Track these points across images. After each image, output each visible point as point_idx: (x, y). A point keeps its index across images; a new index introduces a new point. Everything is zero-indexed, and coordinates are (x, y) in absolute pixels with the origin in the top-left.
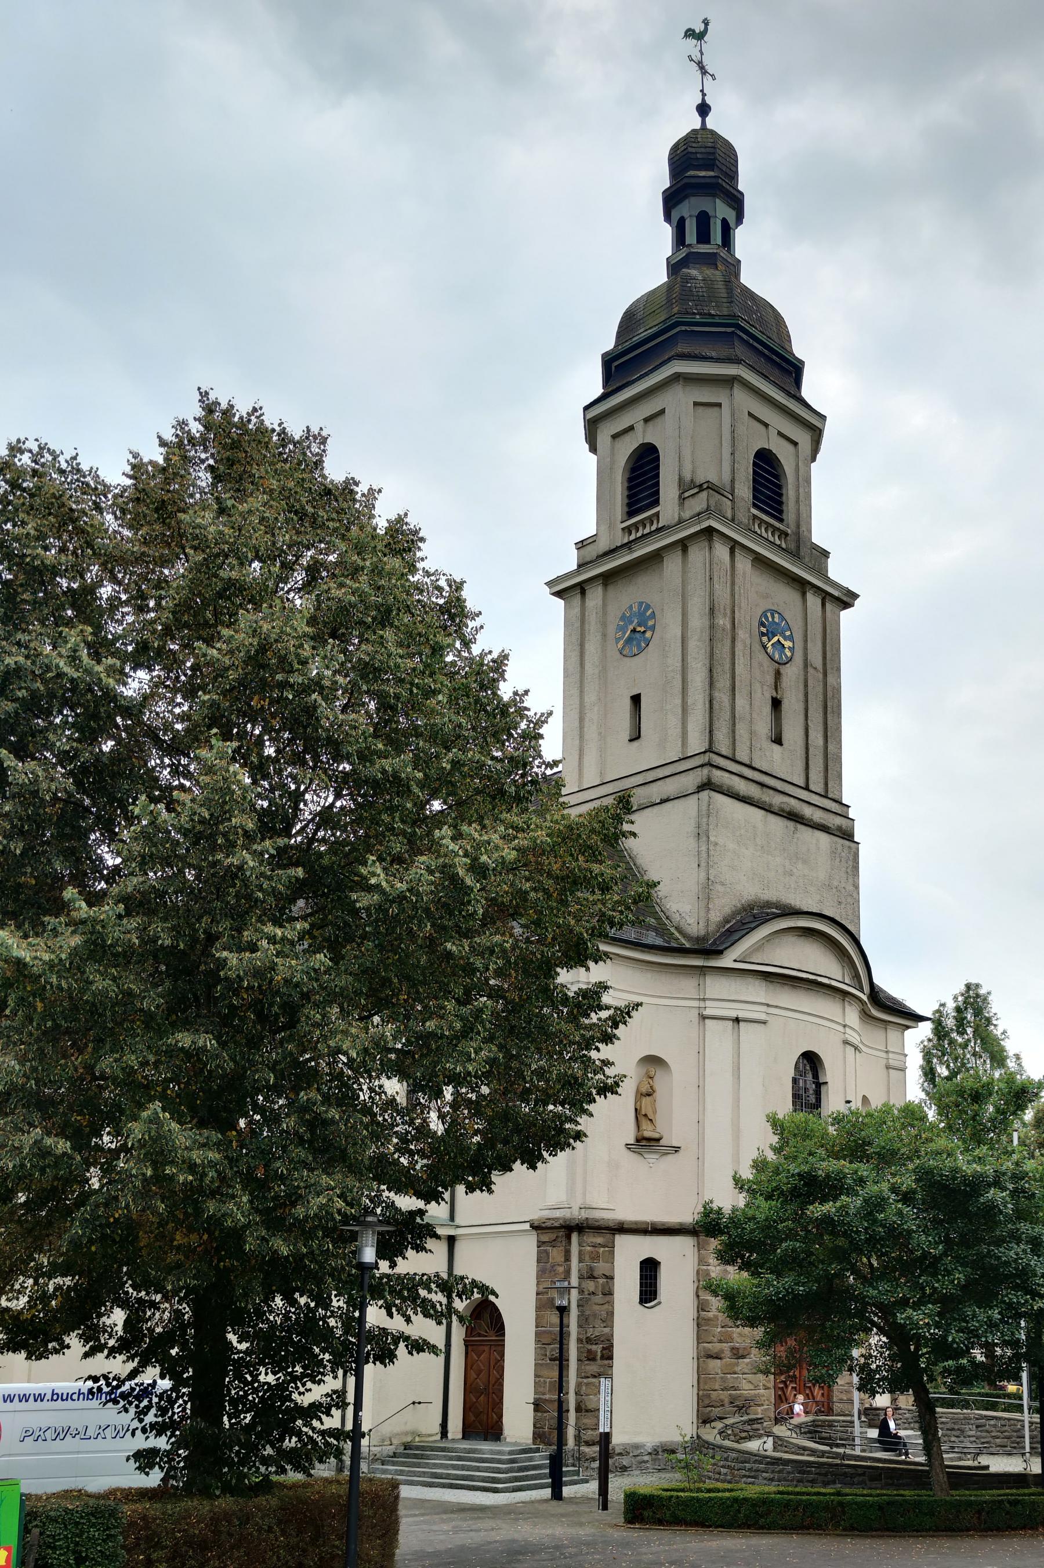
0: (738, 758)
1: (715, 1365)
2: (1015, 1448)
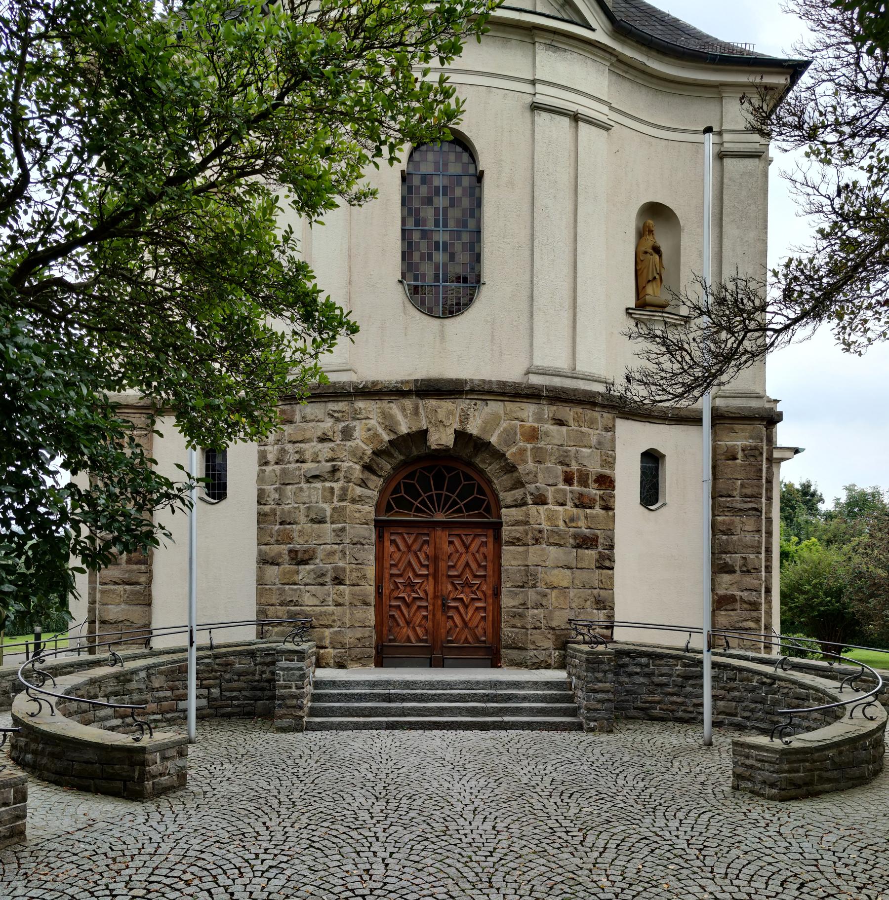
0: (566, 121)
1: (272, 571)
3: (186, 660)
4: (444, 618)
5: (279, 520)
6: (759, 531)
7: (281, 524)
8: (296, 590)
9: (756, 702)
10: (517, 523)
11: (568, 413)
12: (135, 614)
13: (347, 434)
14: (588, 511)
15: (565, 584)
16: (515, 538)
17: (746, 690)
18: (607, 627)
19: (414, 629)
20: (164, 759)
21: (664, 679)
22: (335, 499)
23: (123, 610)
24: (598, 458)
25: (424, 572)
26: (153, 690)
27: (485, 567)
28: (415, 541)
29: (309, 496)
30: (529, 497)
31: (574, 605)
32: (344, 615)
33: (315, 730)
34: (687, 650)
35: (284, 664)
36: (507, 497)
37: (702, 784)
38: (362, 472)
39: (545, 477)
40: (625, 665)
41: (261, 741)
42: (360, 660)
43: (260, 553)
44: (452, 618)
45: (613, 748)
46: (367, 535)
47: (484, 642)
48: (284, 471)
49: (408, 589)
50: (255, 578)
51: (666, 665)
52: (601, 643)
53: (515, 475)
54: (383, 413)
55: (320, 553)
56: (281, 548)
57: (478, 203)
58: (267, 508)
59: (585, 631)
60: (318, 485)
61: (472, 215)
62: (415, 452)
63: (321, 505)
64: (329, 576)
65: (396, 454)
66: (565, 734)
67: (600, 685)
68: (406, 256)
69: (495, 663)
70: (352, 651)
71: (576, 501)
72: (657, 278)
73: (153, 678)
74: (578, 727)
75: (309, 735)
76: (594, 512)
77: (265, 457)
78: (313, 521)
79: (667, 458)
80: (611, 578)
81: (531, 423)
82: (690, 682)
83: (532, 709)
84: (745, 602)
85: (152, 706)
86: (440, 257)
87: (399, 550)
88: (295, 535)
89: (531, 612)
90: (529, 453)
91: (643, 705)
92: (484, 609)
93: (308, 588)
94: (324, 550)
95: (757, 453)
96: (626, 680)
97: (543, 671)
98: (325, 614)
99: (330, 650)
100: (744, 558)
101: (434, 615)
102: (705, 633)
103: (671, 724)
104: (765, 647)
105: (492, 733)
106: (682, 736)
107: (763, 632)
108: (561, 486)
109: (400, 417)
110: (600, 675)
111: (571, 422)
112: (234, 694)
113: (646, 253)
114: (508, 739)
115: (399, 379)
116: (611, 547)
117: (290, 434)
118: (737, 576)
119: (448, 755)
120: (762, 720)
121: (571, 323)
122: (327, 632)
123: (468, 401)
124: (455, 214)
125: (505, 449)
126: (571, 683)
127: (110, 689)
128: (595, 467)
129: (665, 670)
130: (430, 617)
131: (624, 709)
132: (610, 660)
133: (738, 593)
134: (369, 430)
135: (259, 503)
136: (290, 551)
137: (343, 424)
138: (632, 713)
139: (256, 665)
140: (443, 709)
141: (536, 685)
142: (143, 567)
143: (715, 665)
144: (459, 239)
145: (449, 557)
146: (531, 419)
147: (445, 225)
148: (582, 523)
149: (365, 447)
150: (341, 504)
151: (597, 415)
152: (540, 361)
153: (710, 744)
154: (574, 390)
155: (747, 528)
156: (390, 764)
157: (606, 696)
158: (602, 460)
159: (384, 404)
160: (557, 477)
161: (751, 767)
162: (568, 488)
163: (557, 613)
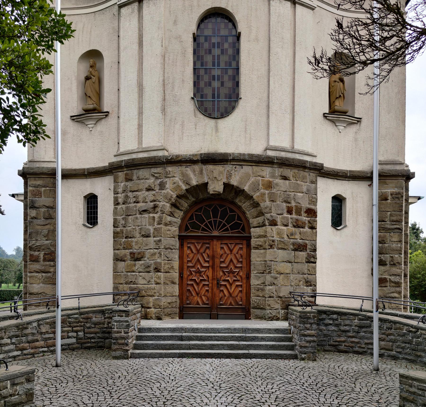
1: (121, 265)
2: (400, 353)
3: (55, 317)
4: (218, 291)
5: (125, 236)
6: (400, 241)
7: (126, 238)
8: (134, 275)
9: (406, 343)
10: (260, 236)
11: (289, 172)
12: (47, 289)
13: (162, 186)
14: (301, 229)
15: (288, 271)
16: (258, 245)
17: (399, 335)
18: (312, 297)
19: (201, 297)
20: (13, 384)
21: (347, 328)
22: (156, 223)
23: (41, 287)
24: (307, 199)
25: (207, 265)
26: (41, 333)
27: (241, 262)
28: (201, 247)
29: (141, 222)
30: (266, 221)
31: (293, 284)
32: (161, 289)
33: (136, 358)
34: (361, 310)
35: (117, 318)
36: (254, 222)
37: (378, 402)
38: (171, 208)
39: (276, 209)
40: (324, 319)
41: (98, 365)
42: (170, 315)
43: (115, 255)
44: (222, 291)
45: (316, 372)
46: (174, 244)
47: (241, 305)
48: (127, 208)
49: (198, 274)
50: (112, 269)
51: (348, 319)
52: (309, 306)
53: (259, 208)
54: (182, 173)
55: (147, 254)
56: (126, 252)
57: (238, 52)
58: (118, 229)
59: (299, 299)
60: (146, 215)
61: (234, 59)
62: (201, 197)
63: (148, 227)
64: (152, 267)
65: (190, 197)
66: (287, 361)
67: (309, 332)
68: (195, 84)
69: (247, 317)
70: (165, 310)
71: (294, 224)
72: (342, 96)
73: (42, 327)
74: (295, 357)
75: (132, 361)
76: (305, 230)
77: (117, 200)
78: (143, 236)
79: (347, 200)
80: (315, 268)
81: (268, 178)
82: (363, 330)
83: (266, 345)
84: (392, 282)
85: (42, 343)
86: (216, 84)
87: (192, 252)
88: (134, 244)
89: (268, 288)
90: (267, 196)
91: (334, 343)
92: (241, 286)
93: (141, 274)
94: (150, 252)
95: (400, 196)
96: (324, 328)
97: (275, 322)
98: (150, 289)
99: (152, 309)
100: (392, 257)
101: (212, 289)
102: (60, 298)
103: (351, 355)
104: (404, 308)
105: (242, 361)
106: (359, 363)
107: (403, 300)
108: (285, 215)
109: (192, 176)
110: (308, 326)
111: (291, 178)
112: (92, 335)
113: (335, 81)
114: (251, 365)
115: (191, 153)
116: (315, 250)
117: (130, 187)
118: (388, 267)
119: (212, 377)
120: (409, 354)
121: (291, 121)
122: (151, 299)
123: (231, 166)
124: (224, 59)
125: (253, 194)
126: (290, 330)
127: (12, 333)
128: (305, 205)
129: (347, 322)
130: (210, 290)
131: (323, 345)
132: (314, 317)
133: (388, 277)
134: (174, 183)
135: (114, 226)
136: (131, 253)
137: (160, 180)
138: (327, 348)
139: (105, 318)
140: (213, 345)
141: (269, 331)
142: (52, 263)
143: (380, 320)
144: (226, 73)
145: (221, 256)
146: (268, 176)
147: (219, 65)
148: (298, 236)
149: (172, 193)
150: (159, 226)
151: (306, 174)
152: (272, 143)
153: (377, 370)
154: (293, 159)
155: (393, 239)
156: (174, 383)
157: (312, 339)
158: (309, 200)
159: (183, 168)
160: (283, 210)
161: (414, 393)
162: (289, 216)
163: (283, 288)
